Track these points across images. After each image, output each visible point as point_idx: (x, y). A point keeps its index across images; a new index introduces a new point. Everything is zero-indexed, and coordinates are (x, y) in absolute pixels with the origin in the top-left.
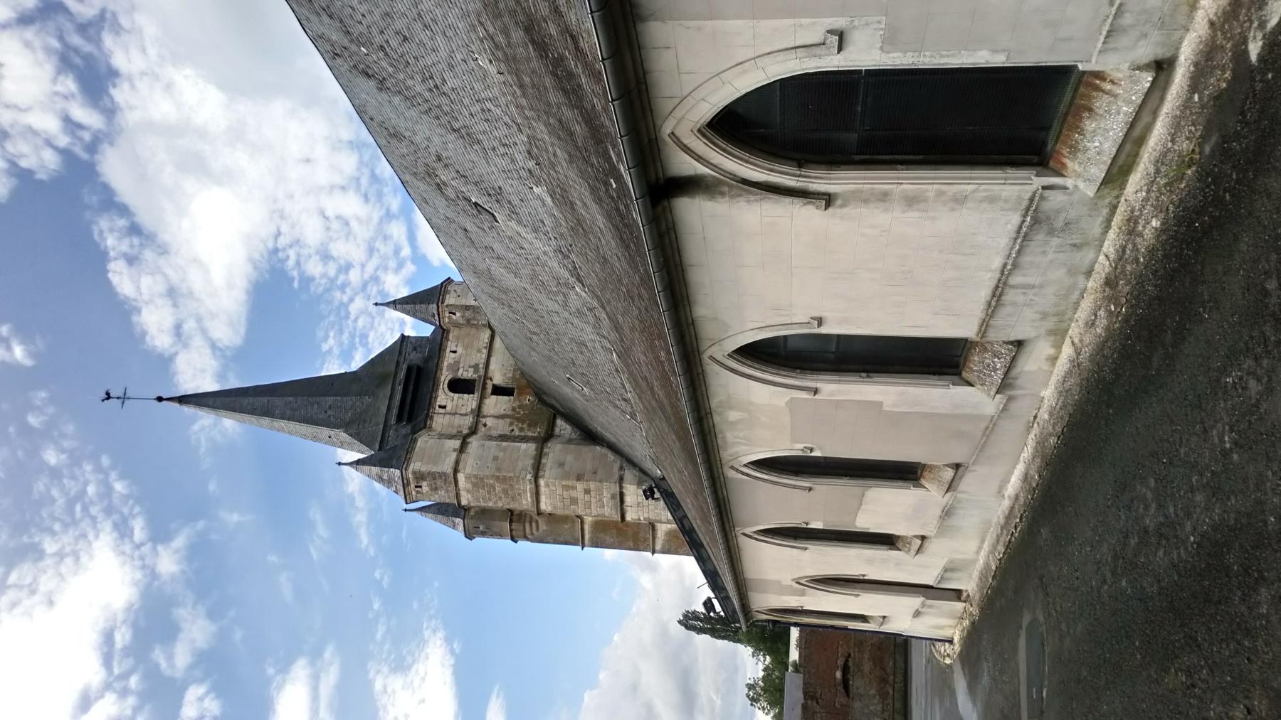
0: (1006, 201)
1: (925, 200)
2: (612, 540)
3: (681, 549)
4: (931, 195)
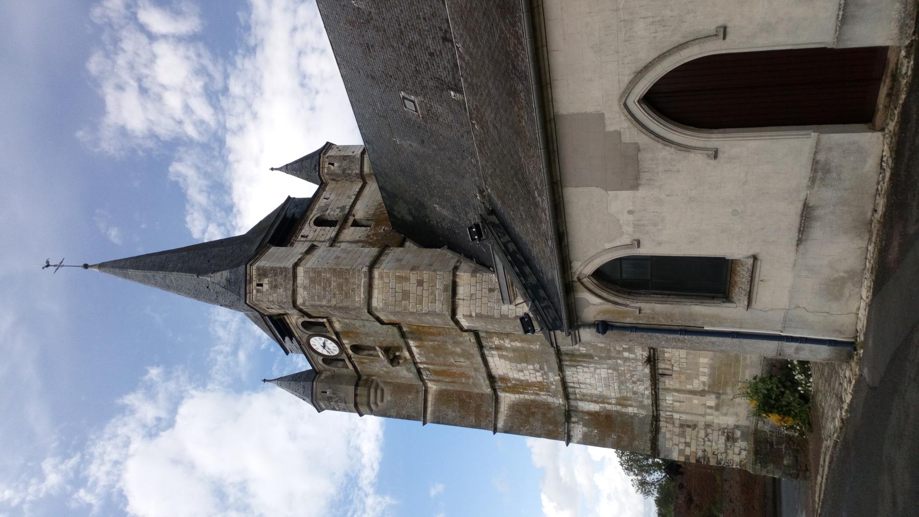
2: (454, 414)
3: (524, 427)
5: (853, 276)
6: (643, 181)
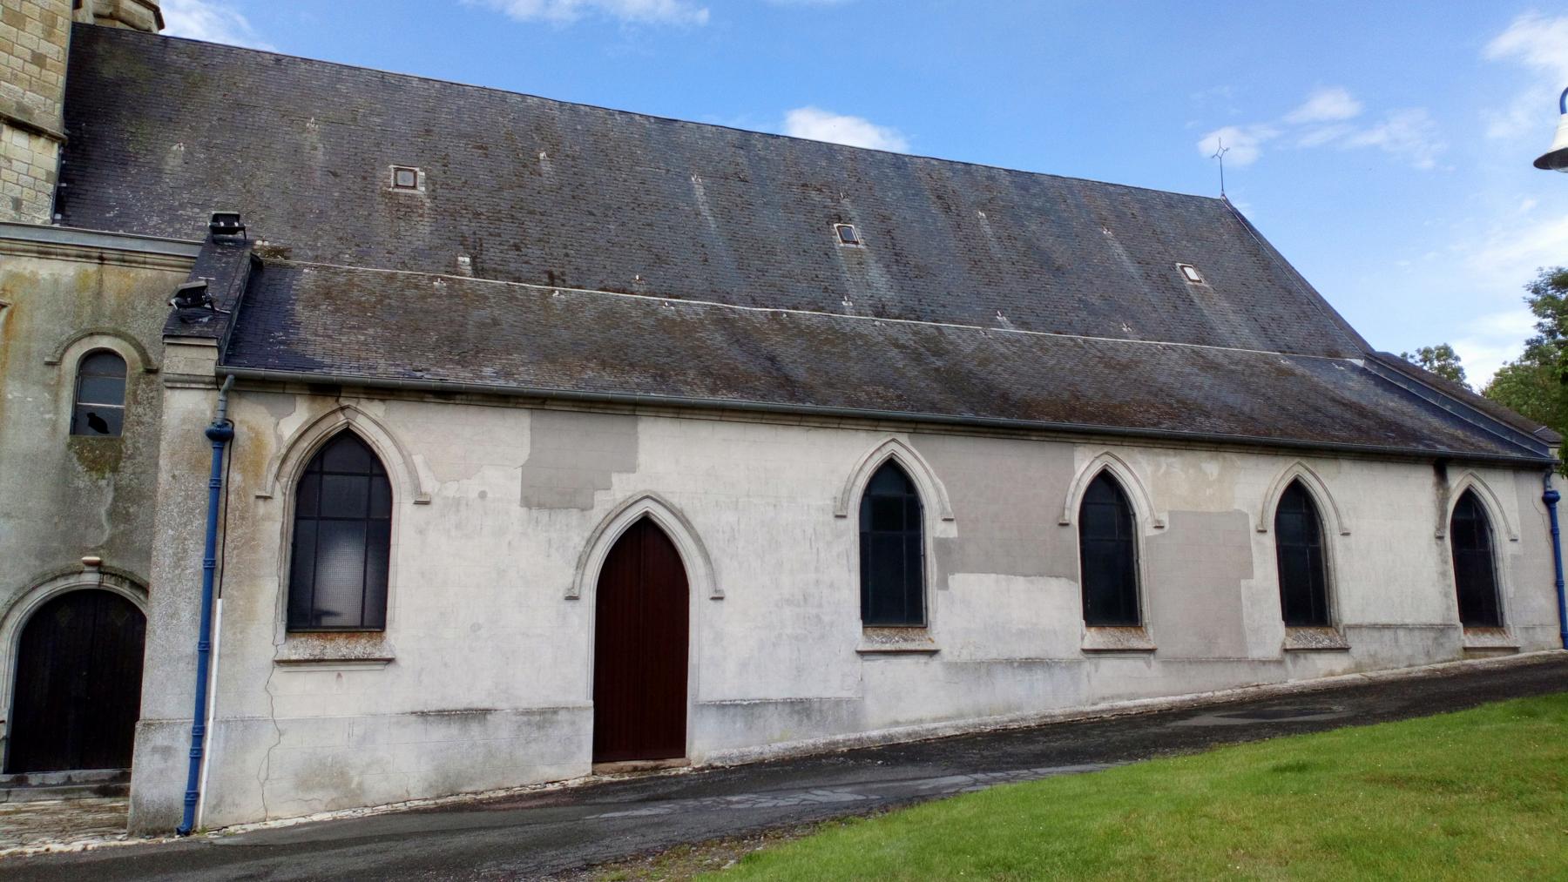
0: (1448, 615)
1: (1444, 580)
4: (1448, 582)
5: (354, 796)
6: (535, 512)
